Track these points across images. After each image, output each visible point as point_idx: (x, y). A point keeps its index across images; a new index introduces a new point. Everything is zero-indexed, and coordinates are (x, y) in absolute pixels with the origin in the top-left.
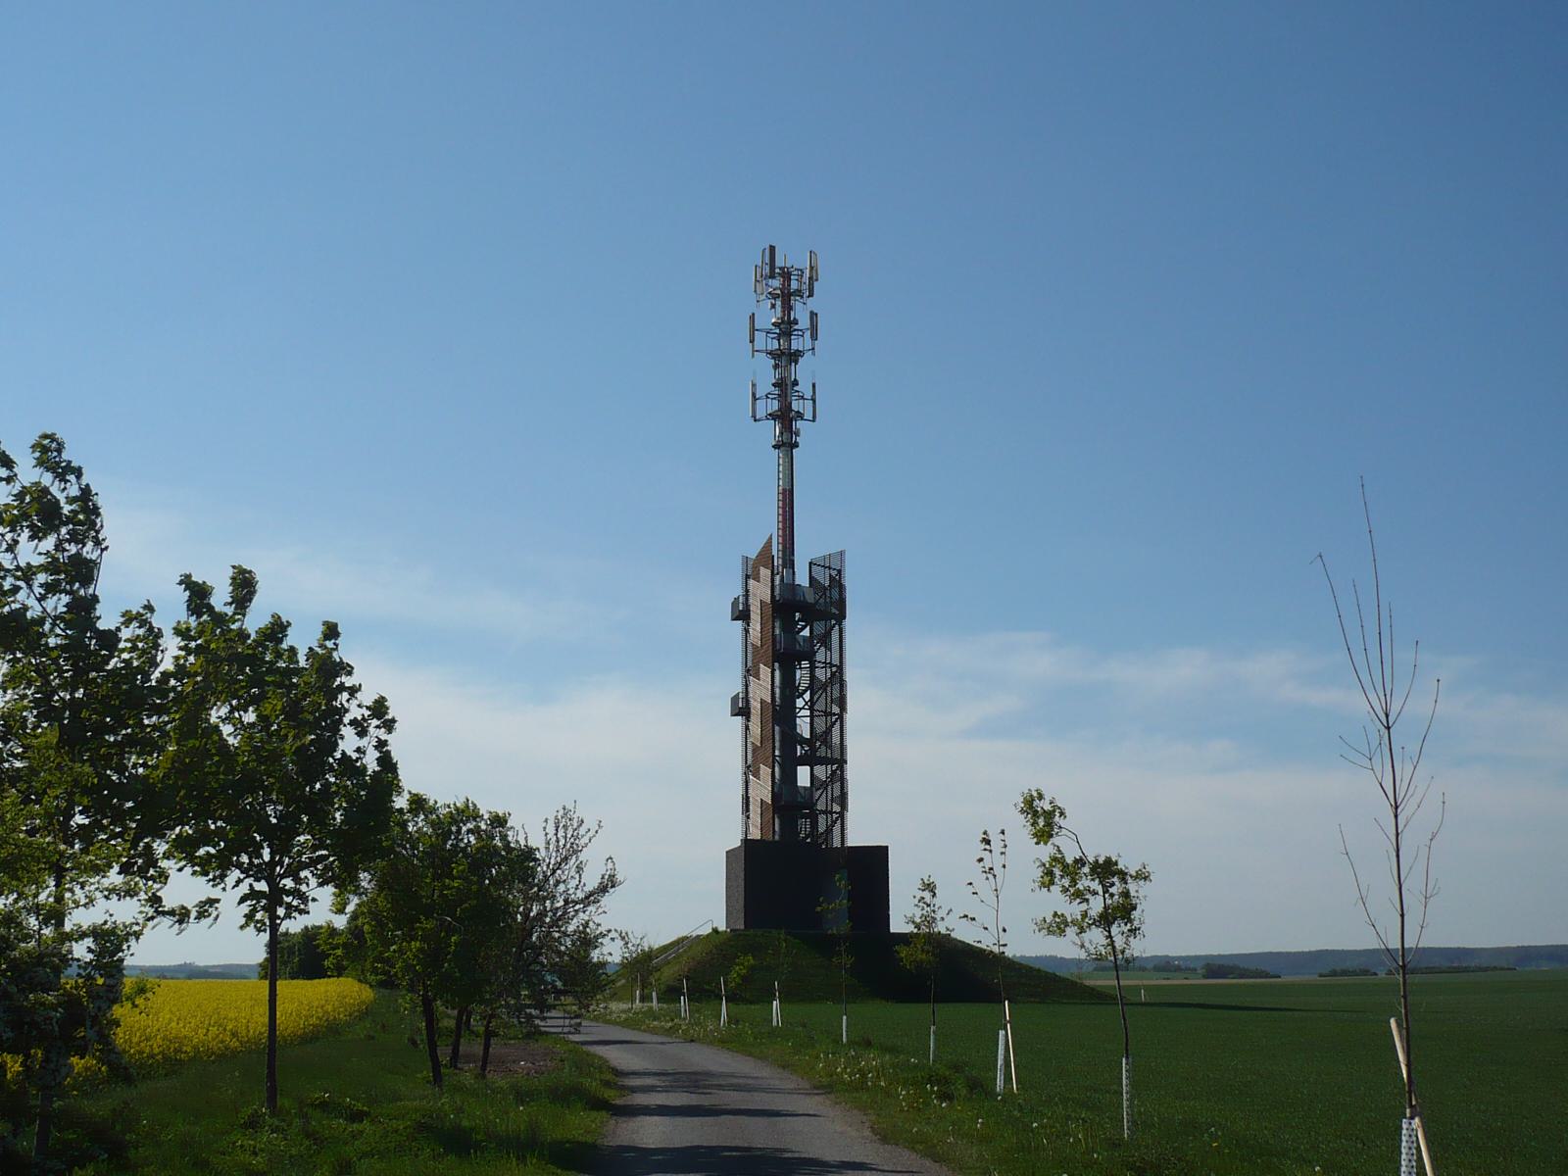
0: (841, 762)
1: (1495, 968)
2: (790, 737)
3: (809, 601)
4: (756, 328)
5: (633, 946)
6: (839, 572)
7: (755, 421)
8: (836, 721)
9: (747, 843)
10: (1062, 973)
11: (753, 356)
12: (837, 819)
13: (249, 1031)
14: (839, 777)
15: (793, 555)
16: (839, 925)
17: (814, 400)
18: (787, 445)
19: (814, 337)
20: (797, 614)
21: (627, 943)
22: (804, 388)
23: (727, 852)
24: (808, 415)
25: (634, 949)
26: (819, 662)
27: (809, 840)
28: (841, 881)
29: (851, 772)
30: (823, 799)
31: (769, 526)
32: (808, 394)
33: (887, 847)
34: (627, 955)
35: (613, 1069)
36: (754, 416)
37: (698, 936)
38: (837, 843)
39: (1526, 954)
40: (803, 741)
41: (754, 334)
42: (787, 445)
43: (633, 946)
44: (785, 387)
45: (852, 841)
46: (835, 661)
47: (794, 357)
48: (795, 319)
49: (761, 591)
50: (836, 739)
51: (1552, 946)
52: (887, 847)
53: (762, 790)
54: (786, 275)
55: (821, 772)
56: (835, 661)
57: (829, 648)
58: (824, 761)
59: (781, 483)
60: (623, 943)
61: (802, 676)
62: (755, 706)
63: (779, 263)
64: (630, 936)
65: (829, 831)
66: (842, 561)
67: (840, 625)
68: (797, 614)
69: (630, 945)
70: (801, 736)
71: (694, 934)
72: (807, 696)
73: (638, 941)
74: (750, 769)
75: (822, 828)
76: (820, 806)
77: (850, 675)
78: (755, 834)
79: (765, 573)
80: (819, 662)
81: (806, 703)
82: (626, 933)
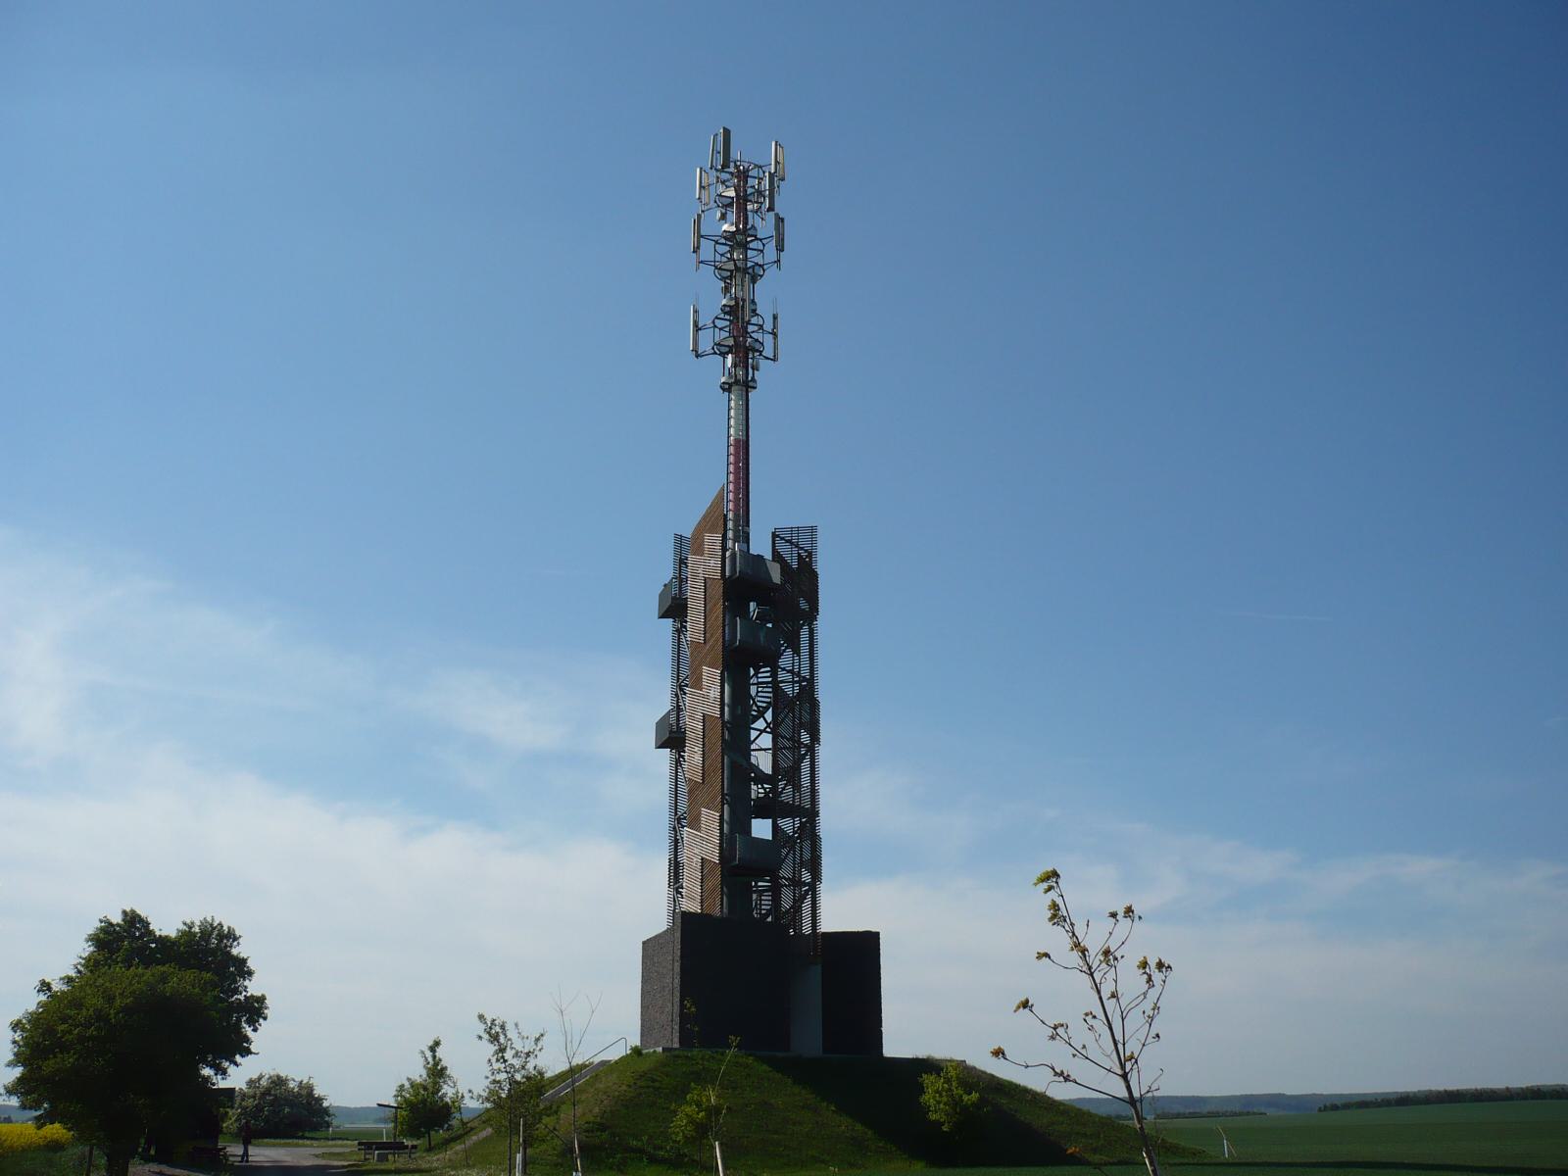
0: (812, 814)
1: (1248, 1113)
2: (741, 771)
3: (775, 581)
4: (702, 233)
5: (517, 1055)
6: (810, 555)
7: (697, 356)
8: (806, 754)
9: (687, 923)
10: (1085, 1108)
11: (697, 269)
12: (807, 892)
13: (794, 1124)
14: (809, 832)
15: (747, 524)
16: (808, 1037)
17: (775, 335)
18: (741, 385)
19: (780, 248)
20: (751, 604)
21: (502, 1050)
22: (764, 309)
23: (644, 943)
24: (768, 352)
25: (517, 1062)
26: (783, 669)
27: (769, 919)
28: (815, 974)
29: (826, 825)
30: (789, 861)
31: (716, 476)
32: (768, 327)
33: (878, 934)
34: (502, 1076)
35: (737, 663)
36: (695, 350)
37: (603, 1063)
38: (807, 929)
39: (1276, 1101)
40: (761, 778)
41: (699, 242)
42: (741, 385)
43: (517, 1055)
44: (738, 314)
45: (827, 925)
46: (805, 673)
47: (752, 274)
48: (753, 226)
49: (707, 566)
50: (805, 781)
51: (1269, 1094)
52: (878, 934)
53: (704, 843)
54: (743, 175)
55: (787, 825)
56: (805, 673)
57: (797, 651)
58: (791, 811)
59: (732, 431)
60: (493, 1048)
61: (759, 691)
62: (693, 726)
63: (735, 154)
64: (512, 1033)
65: (797, 908)
66: (813, 540)
67: (810, 625)
68: (752, 605)
69: (508, 1055)
70: (757, 767)
71: (597, 1060)
72: (769, 715)
73: (529, 1046)
74: (682, 820)
75: (786, 903)
76: (786, 872)
77: (824, 694)
78: (691, 905)
79: (713, 540)
80: (783, 669)
81: (768, 725)
82: (503, 1027)
